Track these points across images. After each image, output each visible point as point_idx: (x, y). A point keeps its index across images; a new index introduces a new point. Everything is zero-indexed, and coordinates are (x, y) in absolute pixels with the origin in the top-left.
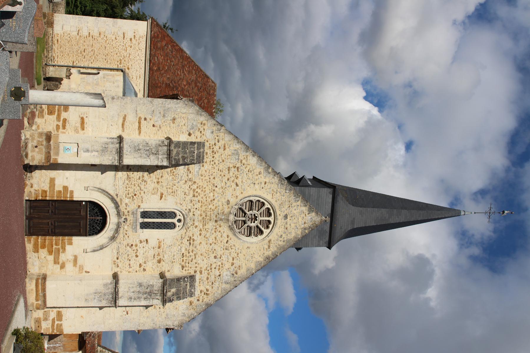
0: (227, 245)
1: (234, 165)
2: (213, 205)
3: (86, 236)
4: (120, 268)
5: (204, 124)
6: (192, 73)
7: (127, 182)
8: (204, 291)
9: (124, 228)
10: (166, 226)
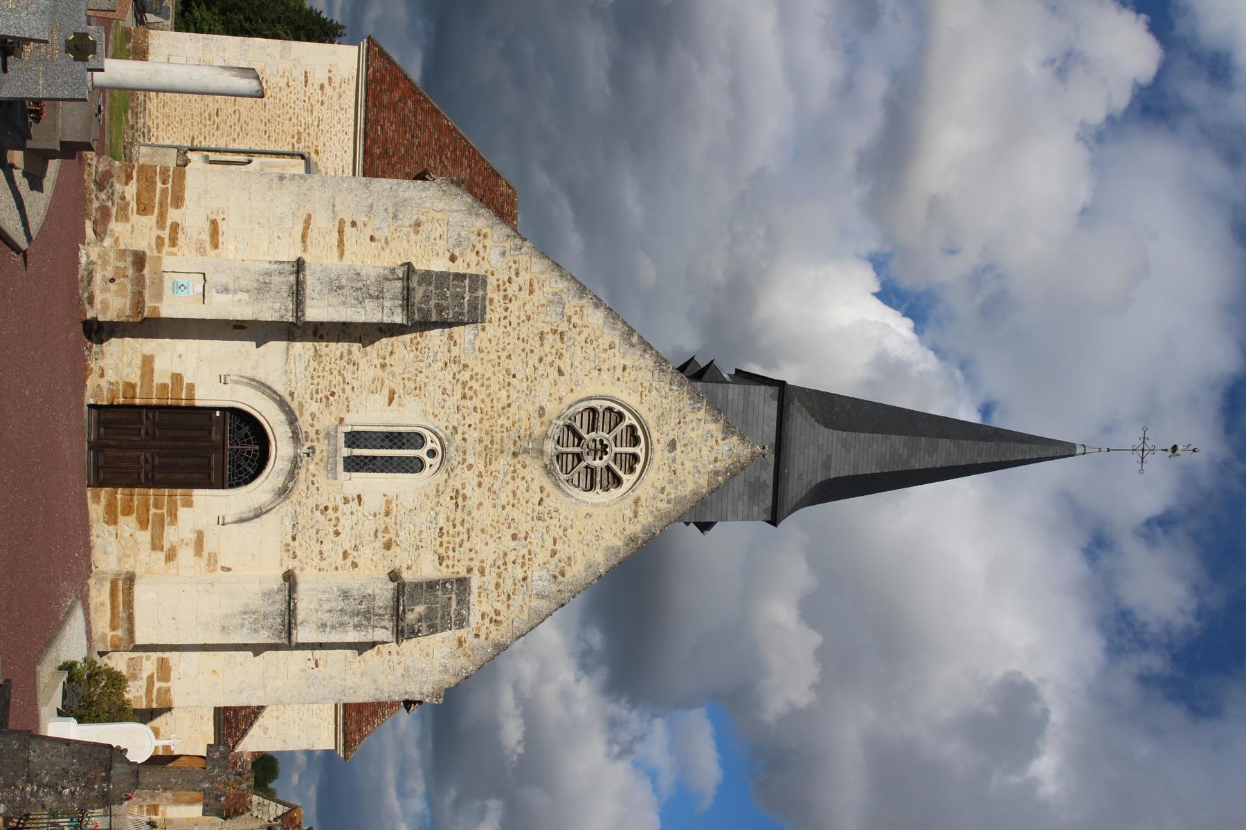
0: (541, 508)
1: (553, 328)
2: (508, 418)
3: (223, 488)
4: (300, 560)
5: (485, 236)
6: (462, 164)
7: (314, 364)
8: (490, 616)
9: (308, 470)
10: (403, 465)
